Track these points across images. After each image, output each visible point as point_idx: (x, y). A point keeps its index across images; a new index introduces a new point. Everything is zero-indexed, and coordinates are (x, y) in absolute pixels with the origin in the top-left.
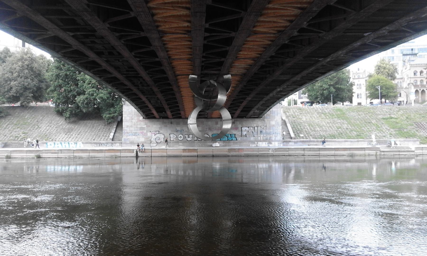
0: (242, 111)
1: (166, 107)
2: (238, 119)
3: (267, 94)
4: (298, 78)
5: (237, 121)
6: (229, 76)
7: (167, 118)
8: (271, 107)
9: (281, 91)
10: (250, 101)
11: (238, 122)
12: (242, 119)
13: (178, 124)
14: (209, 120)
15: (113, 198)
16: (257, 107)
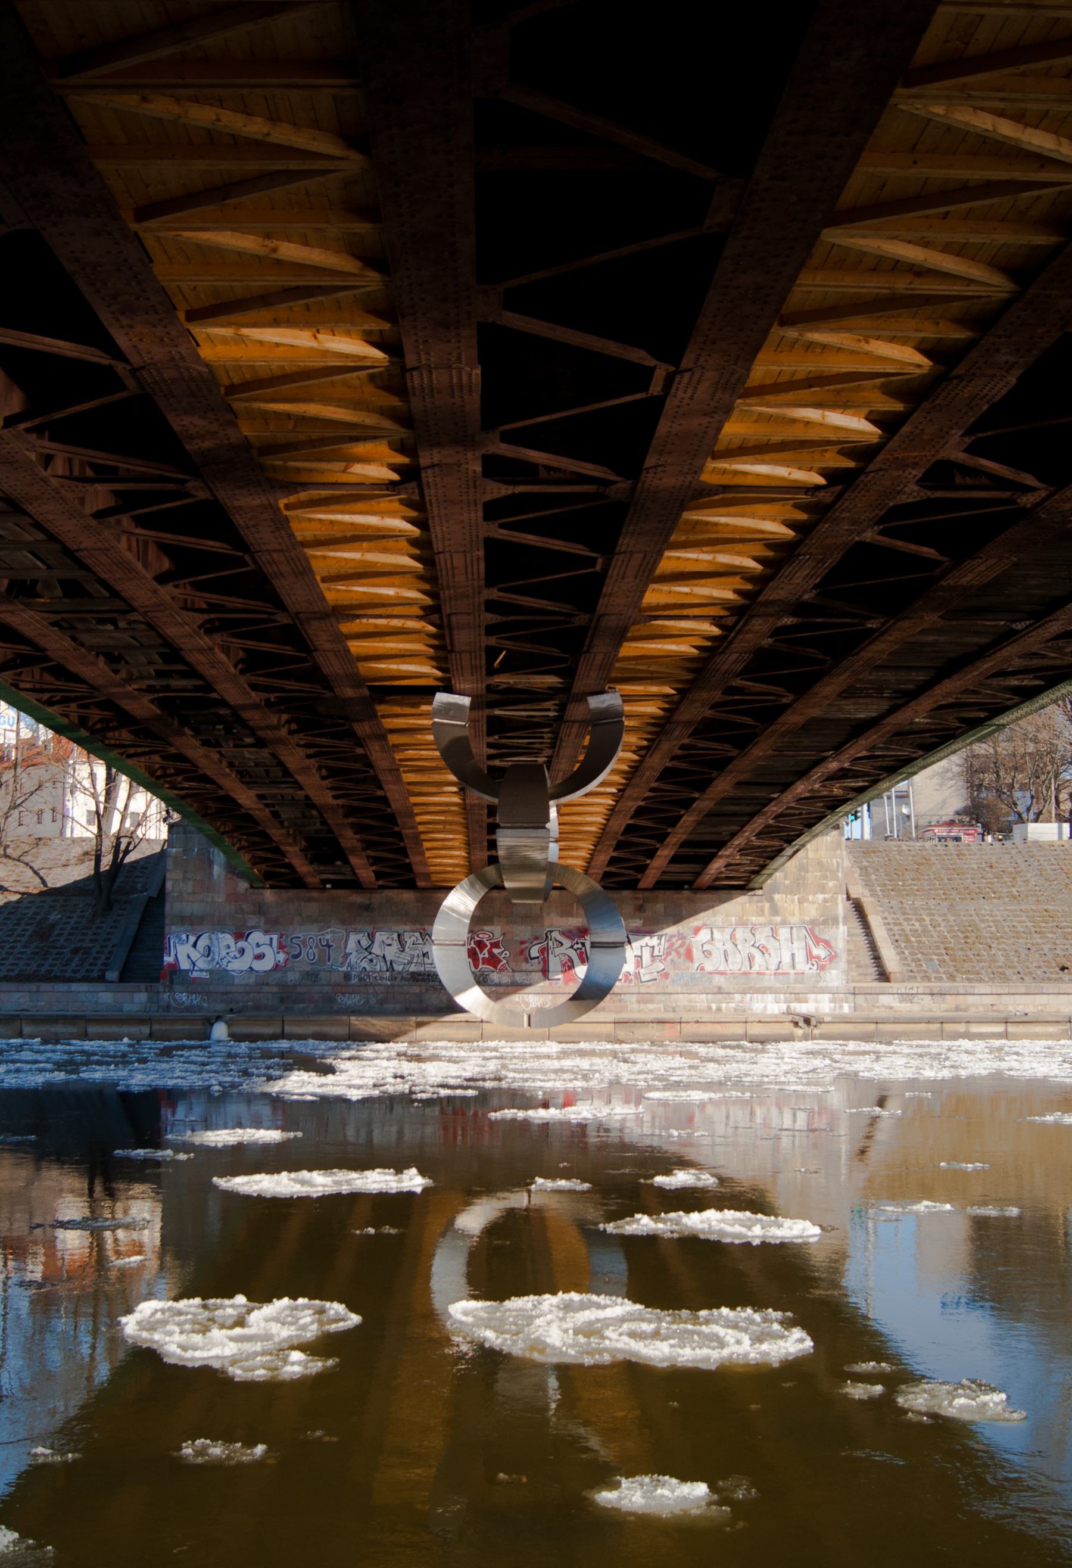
0: (675, 860)
1: (349, 839)
3: (785, 787)
4: (918, 715)
7: (354, 884)
8: (799, 841)
9: (842, 774)
10: (711, 814)
16: (738, 841)
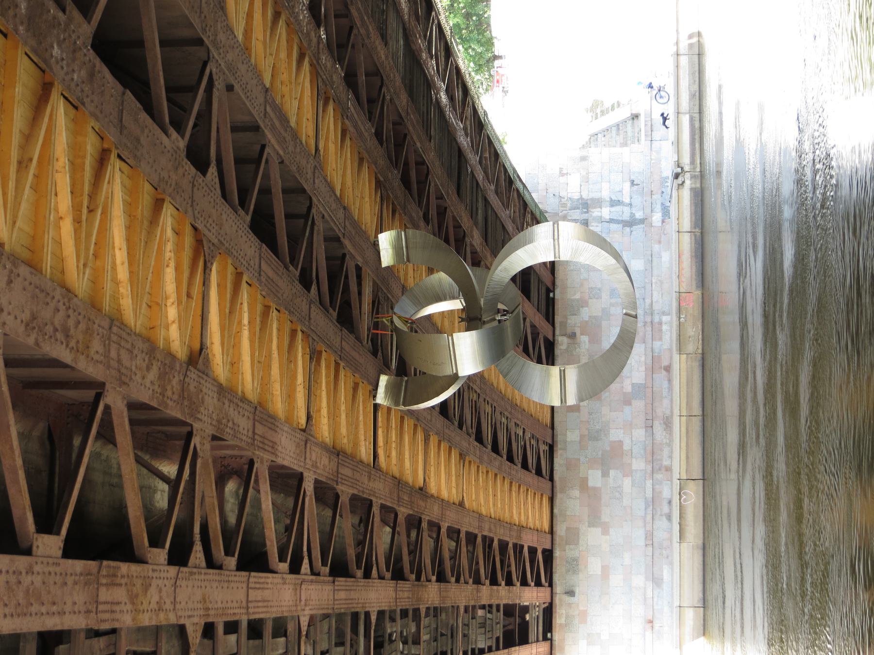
2: (558, 319)
5: (564, 324)
6: (385, 240)
11: (572, 321)
12: (559, 306)
13: (574, 565)
14: (559, 438)
15: (818, 166)
